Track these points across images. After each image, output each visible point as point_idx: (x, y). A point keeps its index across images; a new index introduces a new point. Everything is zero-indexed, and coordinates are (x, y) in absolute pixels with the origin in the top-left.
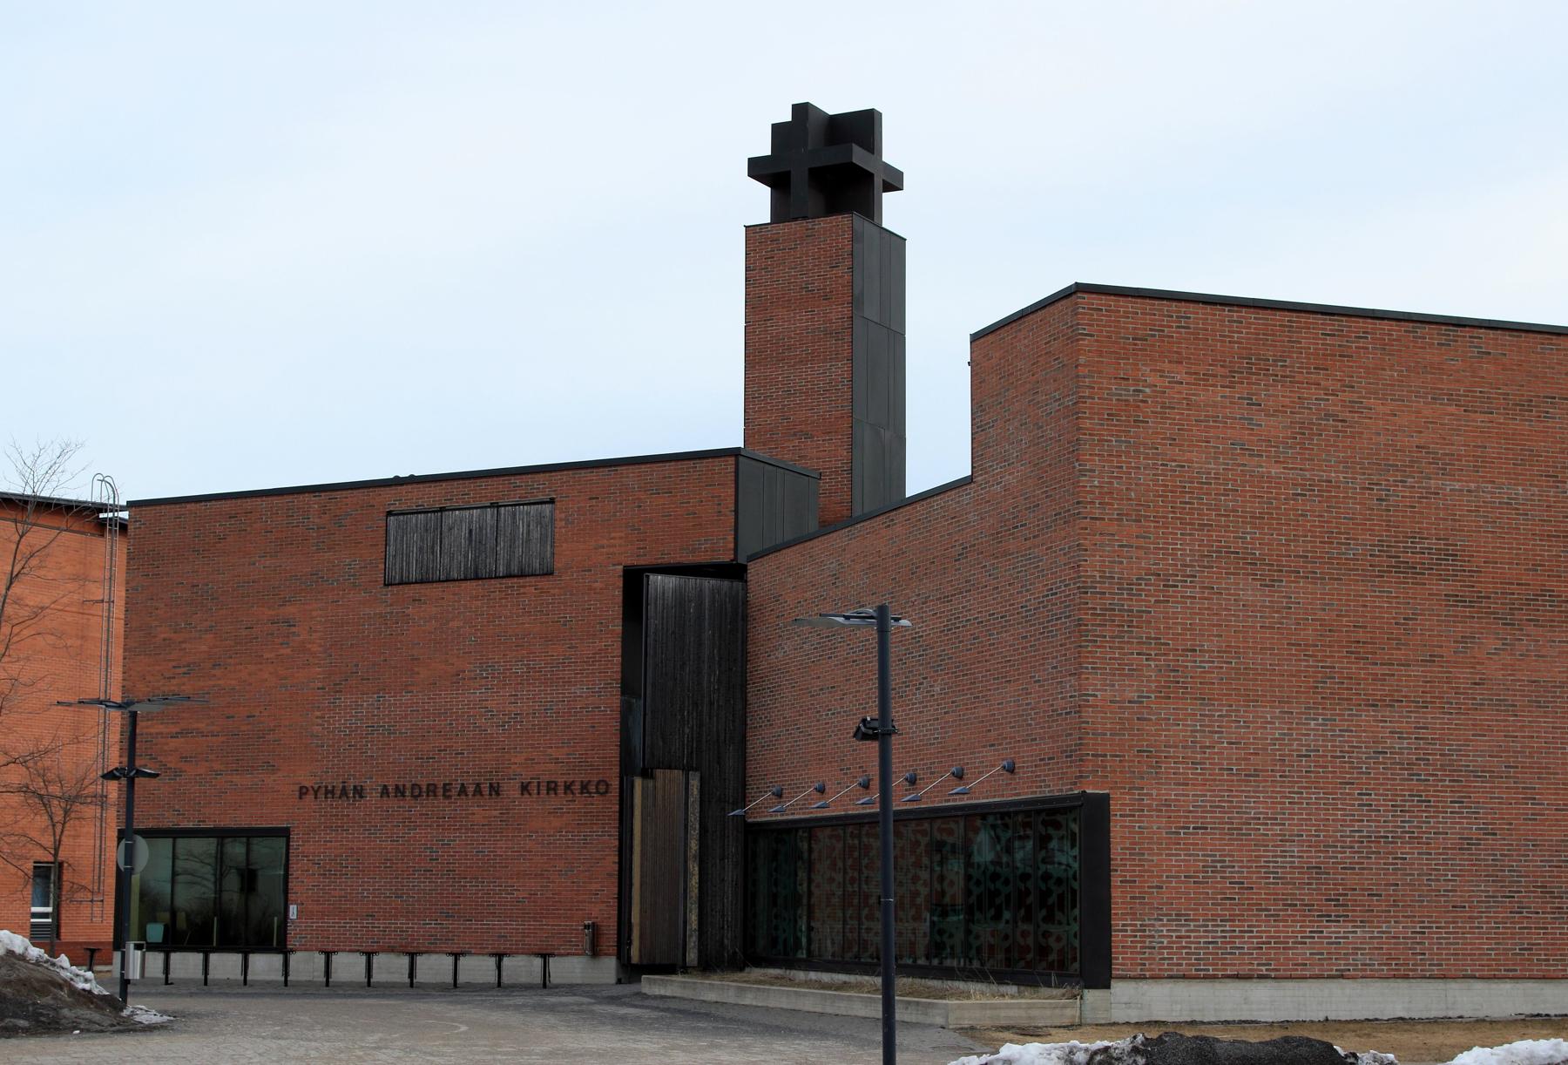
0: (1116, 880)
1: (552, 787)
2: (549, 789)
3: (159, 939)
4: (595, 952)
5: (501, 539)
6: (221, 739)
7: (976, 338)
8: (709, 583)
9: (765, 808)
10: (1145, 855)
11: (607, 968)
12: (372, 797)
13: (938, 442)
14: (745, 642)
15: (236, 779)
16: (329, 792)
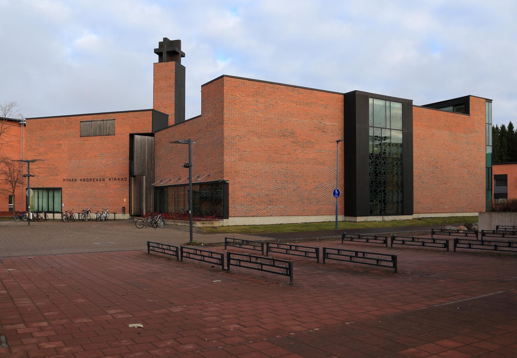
0: (230, 197)
1: (115, 179)
7: (202, 86)
8: (147, 137)
9: (158, 183)
10: (235, 193)
11: (127, 216)
12: (78, 181)
13: (193, 108)
15: (50, 177)
16: (70, 180)
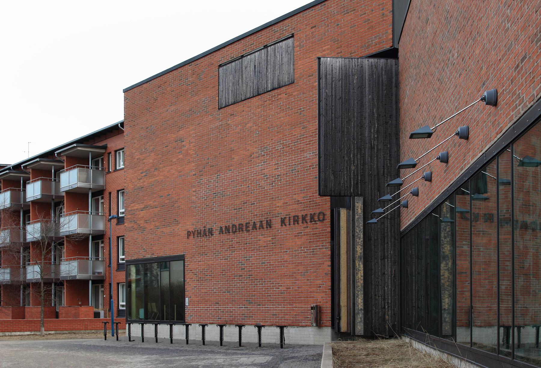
1: (296, 220)
2: (294, 221)
3: (362, 333)
4: (319, 324)
5: (269, 66)
6: (158, 209)
14: (397, 102)
15: (164, 230)
16: (199, 233)
